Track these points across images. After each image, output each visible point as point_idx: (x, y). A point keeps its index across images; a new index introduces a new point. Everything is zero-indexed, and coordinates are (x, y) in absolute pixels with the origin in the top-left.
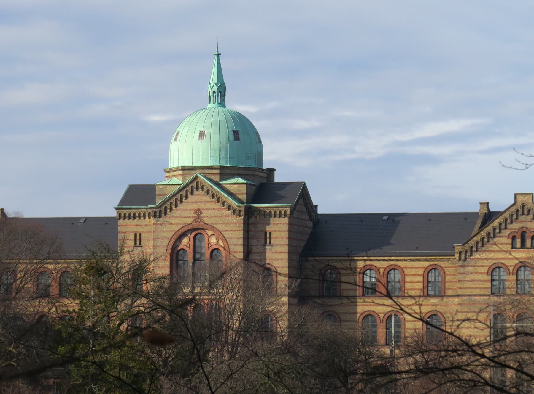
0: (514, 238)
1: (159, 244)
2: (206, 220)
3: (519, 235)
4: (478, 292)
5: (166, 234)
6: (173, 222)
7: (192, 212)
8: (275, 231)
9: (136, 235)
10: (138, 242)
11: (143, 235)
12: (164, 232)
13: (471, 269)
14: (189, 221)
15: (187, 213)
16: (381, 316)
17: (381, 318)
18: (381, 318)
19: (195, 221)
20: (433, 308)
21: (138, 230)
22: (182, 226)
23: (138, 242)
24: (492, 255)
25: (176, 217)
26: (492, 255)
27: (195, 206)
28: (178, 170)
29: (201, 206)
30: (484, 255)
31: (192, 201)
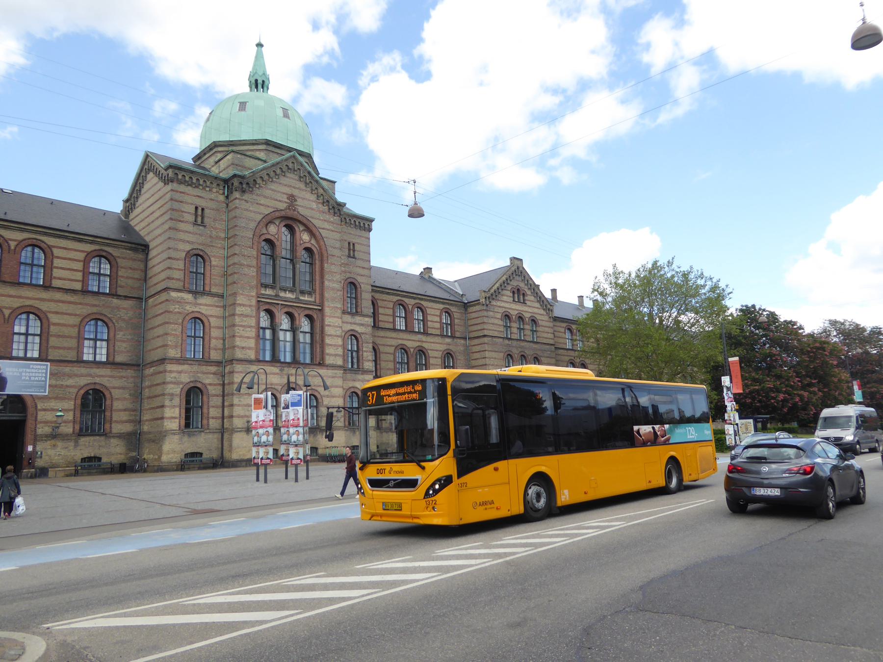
0: (514, 293)
1: (243, 225)
2: (301, 210)
3: (516, 291)
4: (496, 334)
5: (252, 215)
6: (262, 202)
7: (285, 196)
8: (358, 244)
9: (196, 208)
10: (199, 219)
11: (206, 211)
12: (251, 211)
13: (491, 314)
14: (282, 206)
15: (279, 196)
16: (412, 350)
17: (7, 316)
18: (7, 316)
19: (288, 208)
20: (448, 347)
21: (201, 203)
22: (272, 210)
23: (199, 219)
24: (503, 304)
25: (265, 197)
26: (503, 304)
27: (288, 191)
28: (262, 144)
29: (296, 192)
30: (499, 304)
31: (285, 183)
